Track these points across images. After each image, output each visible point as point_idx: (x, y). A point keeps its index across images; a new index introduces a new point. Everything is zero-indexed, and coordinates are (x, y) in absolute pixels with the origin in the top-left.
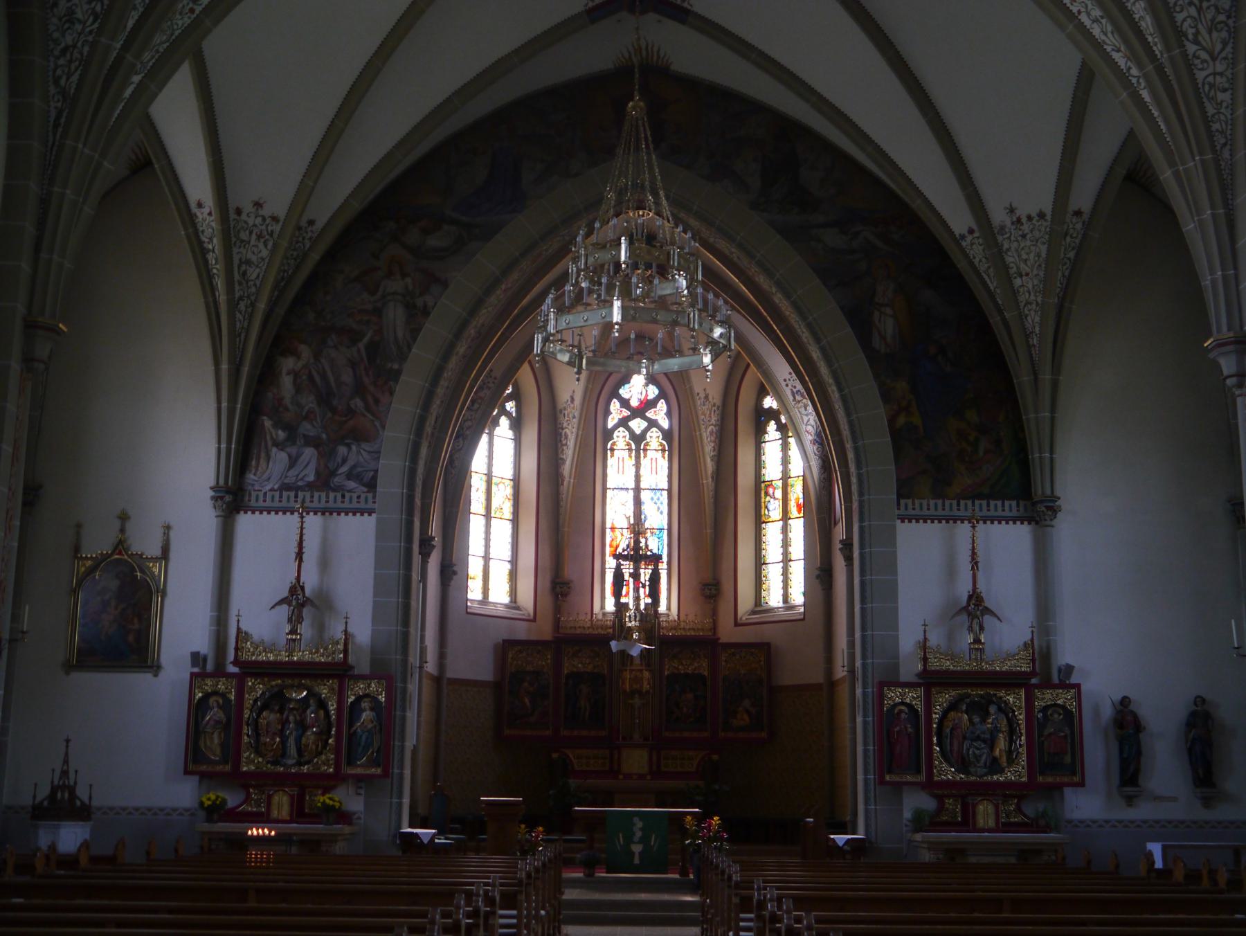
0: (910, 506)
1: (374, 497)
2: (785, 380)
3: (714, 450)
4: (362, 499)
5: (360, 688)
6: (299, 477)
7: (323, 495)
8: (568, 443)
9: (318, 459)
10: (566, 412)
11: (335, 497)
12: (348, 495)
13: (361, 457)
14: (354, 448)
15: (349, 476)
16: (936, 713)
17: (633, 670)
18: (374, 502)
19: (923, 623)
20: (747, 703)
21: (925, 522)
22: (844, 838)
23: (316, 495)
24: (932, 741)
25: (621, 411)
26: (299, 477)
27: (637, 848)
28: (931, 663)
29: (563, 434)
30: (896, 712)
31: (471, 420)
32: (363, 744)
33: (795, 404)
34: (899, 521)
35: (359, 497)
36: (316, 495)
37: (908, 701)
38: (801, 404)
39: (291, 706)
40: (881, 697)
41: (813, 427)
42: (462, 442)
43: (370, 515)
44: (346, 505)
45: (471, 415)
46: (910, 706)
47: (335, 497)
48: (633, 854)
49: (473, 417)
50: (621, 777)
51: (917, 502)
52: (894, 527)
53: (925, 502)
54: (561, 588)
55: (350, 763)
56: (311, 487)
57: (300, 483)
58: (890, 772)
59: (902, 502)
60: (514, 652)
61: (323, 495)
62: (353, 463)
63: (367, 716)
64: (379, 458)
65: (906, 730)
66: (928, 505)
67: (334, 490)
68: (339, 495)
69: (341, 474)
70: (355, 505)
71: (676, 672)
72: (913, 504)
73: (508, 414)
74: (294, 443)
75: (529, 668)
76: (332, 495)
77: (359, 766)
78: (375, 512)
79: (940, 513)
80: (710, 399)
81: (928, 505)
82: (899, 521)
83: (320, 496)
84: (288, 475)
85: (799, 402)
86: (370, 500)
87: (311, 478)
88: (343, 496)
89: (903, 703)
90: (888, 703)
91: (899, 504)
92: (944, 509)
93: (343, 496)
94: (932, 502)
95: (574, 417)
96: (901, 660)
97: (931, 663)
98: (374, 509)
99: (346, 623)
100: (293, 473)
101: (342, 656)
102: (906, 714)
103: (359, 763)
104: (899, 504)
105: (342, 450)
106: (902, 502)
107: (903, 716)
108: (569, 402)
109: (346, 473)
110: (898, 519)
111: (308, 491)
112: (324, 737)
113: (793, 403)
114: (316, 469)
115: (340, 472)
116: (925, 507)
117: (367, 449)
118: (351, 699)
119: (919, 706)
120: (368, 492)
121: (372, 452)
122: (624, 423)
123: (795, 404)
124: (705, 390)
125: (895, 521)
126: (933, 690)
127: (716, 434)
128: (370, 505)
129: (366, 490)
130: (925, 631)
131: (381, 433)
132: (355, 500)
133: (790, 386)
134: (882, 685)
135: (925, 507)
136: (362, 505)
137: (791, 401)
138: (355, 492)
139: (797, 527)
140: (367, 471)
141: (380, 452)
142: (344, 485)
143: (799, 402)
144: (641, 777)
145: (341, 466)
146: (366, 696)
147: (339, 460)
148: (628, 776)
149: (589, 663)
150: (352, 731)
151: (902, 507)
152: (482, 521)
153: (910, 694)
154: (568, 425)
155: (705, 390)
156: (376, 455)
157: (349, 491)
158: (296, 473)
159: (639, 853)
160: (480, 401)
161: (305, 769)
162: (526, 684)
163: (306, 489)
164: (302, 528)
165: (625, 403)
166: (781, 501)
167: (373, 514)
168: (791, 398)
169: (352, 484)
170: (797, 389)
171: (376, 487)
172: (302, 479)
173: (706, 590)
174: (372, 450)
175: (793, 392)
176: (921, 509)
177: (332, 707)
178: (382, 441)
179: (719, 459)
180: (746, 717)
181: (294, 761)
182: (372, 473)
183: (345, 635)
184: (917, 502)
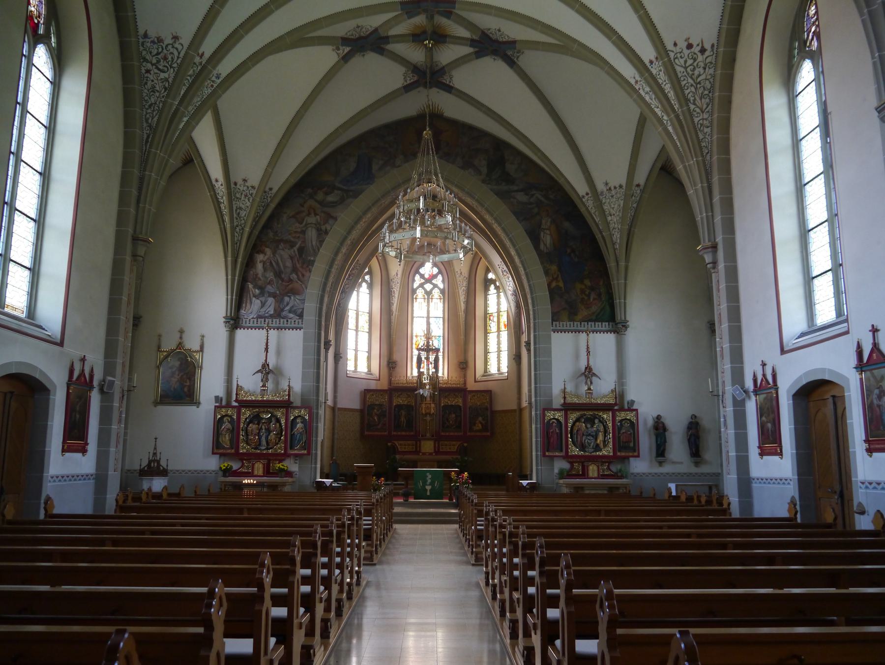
0: (558, 325)
1: (302, 322)
4: (296, 322)
5: (296, 412)
6: (266, 312)
7: (278, 320)
12: (289, 320)
14: (292, 298)
20: (480, 419)
23: (274, 320)
24: (568, 436)
27: (428, 488)
35: (295, 321)
36: (274, 320)
40: (544, 415)
44: (289, 325)
46: (557, 420)
47: (283, 322)
48: (427, 490)
51: (561, 323)
53: (565, 323)
56: (271, 316)
58: (548, 451)
59: (554, 323)
61: (278, 320)
66: (566, 325)
67: (283, 318)
68: (285, 320)
70: (293, 325)
72: (559, 324)
74: (263, 296)
75: (377, 403)
77: (296, 449)
80: (463, 274)
81: (566, 325)
85: (505, 275)
86: (300, 323)
87: (272, 312)
88: (287, 321)
89: (554, 419)
91: (552, 324)
93: (287, 321)
94: (568, 323)
96: (553, 398)
101: (287, 397)
104: (552, 324)
105: (286, 299)
106: (554, 323)
107: (554, 424)
112: (279, 436)
115: (285, 309)
119: (562, 419)
128: (300, 325)
129: (298, 318)
136: (296, 325)
139: (504, 335)
143: (505, 275)
144: (431, 454)
147: (285, 303)
148: (424, 454)
156: (303, 301)
157: (290, 319)
159: (430, 490)
161: (270, 451)
162: (375, 411)
165: (422, 276)
168: (502, 274)
169: (291, 315)
172: (267, 313)
174: (301, 299)
177: (283, 422)
180: (480, 425)
182: (301, 310)
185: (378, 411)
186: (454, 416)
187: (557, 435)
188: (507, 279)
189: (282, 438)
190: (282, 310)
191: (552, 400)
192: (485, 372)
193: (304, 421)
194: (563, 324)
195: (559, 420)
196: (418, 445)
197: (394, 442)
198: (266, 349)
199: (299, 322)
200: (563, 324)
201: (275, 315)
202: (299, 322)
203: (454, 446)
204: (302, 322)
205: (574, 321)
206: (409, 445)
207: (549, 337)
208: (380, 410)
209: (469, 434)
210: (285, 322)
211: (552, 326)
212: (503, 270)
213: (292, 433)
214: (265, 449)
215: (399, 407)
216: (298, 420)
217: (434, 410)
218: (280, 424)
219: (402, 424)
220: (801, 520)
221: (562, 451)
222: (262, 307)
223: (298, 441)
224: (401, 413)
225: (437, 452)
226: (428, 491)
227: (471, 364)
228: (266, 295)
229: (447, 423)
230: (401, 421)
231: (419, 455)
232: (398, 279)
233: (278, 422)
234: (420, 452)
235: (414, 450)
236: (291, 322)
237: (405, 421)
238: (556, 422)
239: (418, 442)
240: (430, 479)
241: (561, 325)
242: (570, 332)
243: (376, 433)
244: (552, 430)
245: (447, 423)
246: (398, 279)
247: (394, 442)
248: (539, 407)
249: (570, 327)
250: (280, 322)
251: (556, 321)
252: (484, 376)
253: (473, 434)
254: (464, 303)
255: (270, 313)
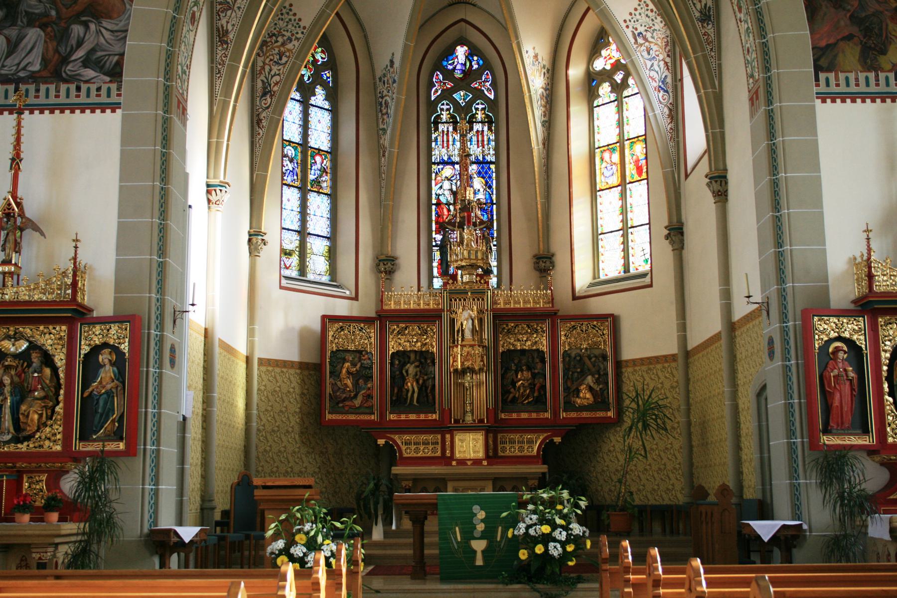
0: (833, 82)
1: (119, 89)
2: (625, 21)
3: (545, 116)
4: (104, 92)
5: (95, 335)
6: (22, 65)
7: (52, 87)
8: (389, 111)
9: (45, 42)
10: (386, 79)
11: (68, 90)
12: (84, 87)
13: (101, 38)
14: (93, 27)
15: (86, 63)
16: (886, 351)
17: (465, 346)
18: (119, 95)
19: (865, 228)
20: (589, 379)
21: (854, 101)
22: (776, 525)
23: (43, 87)
24: (883, 388)
25: (445, 84)
26: (22, 65)
27: (479, 545)
28: (879, 282)
29: (383, 103)
30: (830, 350)
31: (279, 75)
32: (100, 410)
33: (637, 47)
34: (820, 100)
35: (99, 89)
36: (43, 87)
37: (847, 335)
38: (643, 48)
39: (6, 363)
40: (807, 331)
41: (657, 73)
42: (269, 100)
43: (113, 111)
44: (83, 99)
45: (279, 70)
46: (849, 342)
47: (68, 90)
48: (475, 552)
49: (281, 72)
50: (454, 463)
51: (842, 76)
52: (814, 106)
53: (852, 76)
54: (384, 264)
55: (84, 437)
56: (34, 78)
57: (22, 74)
58: (826, 431)
59: (822, 76)
60: (335, 329)
61: (52, 87)
62: (92, 46)
63: (107, 373)
64: (126, 37)
65: (847, 376)
66: (857, 79)
67: (66, 81)
68: (73, 87)
69: (76, 60)
70: (93, 99)
71: (512, 348)
72: (837, 79)
73: (325, 85)
74: (14, 24)
75: (352, 347)
76: (63, 87)
77: (95, 440)
78: (120, 108)
79: (873, 88)
80: (540, 60)
81: (857, 79)
82: (820, 100)
83: (48, 90)
84: (5, 64)
85: (641, 45)
86: (114, 92)
87: (36, 67)
88: (78, 89)
89: (839, 339)
90: (819, 339)
91: (817, 79)
92: (877, 85)
93: (78, 89)
94: (862, 76)
95: (394, 82)
96: (830, 283)
97: (879, 282)
98: (120, 104)
99: (76, 247)
100: (11, 61)
101: (69, 291)
102: (845, 352)
103: (94, 437)
104: (817, 79)
105: (77, 30)
106: (822, 76)
107: (841, 355)
108: (389, 68)
109: (81, 60)
110: (817, 98)
111: (32, 83)
112: (51, 404)
113: (635, 46)
114: (43, 55)
115: (73, 58)
116: (852, 82)
117: (109, 27)
118: (85, 349)
119: (860, 340)
120: (111, 82)
121: (117, 31)
122: (447, 95)
123: (637, 47)
124: (534, 48)
125: (814, 102)
126: (880, 320)
127: (546, 98)
128: (114, 99)
129: (108, 79)
130: (868, 239)
131: (128, 6)
132: (94, 92)
133: (631, 27)
134: (807, 316)
135: (852, 82)
136: (104, 99)
137: (633, 43)
138: (94, 83)
139: (639, 193)
140: (110, 55)
141: (127, 31)
142: (79, 75)
143: (641, 45)
144: (477, 462)
145: (76, 50)
146: (105, 345)
147: (73, 42)
148: (462, 462)
149: (417, 342)
150: (86, 394)
151: (822, 81)
152: (312, 228)
153: (849, 326)
154: (388, 92)
155: (534, 48)
156: (122, 35)
157: (87, 82)
158: (16, 61)
159: (483, 552)
160: (288, 54)
161: (23, 447)
162: (347, 365)
163: (30, 81)
164: (18, 132)
165: (449, 75)
166: (619, 166)
167: (118, 110)
168: (633, 41)
169: (90, 73)
170: (638, 31)
171: (122, 76)
172: (24, 69)
173: (541, 262)
174: (116, 28)
175: (634, 34)
176: (848, 85)
177: (60, 360)
178: (130, 16)
179: (549, 124)
180: (588, 395)
181: (10, 436)
182: (116, 58)
183: (75, 263)
184: (842, 76)
185: (354, 365)
186: (527, 374)
187: (851, 384)
188: (645, 54)
189: (57, 409)
190: (65, 60)
191: (827, 287)
192: (594, 278)
193: (119, 361)
194: (847, 79)
195: (854, 342)
196: (448, 443)
197: (392, 436)
198: (13, 160)
199: (109, 90)
200: (847, 79)
201: (45, 74)
202: (109, 90)
203: (534, 444)
204: (119, 89)
205: (876, 68)
206: (426, 443)
207: (812, 112)
208: (359, 365)
209: (563, 415)
210: (73, 92)
211: (818, 85)
212: (636, 32)
213: (86, 394)
214: (8, 442)
215: (402, 357)
216: (104, 357)
217: (482, 361)
218: (55, 370)
219: (409, 395)
220: (410, 538)
221: (866, 431)
222: (10, 53)
223: (102, 415)
224: (407, 371)
225: (492, 455)
226: (479, 556)
227: (561, 260)
228: (22, 20)
229: (512, 390)
230: (408, 391)
231: (451, 465)
232: (393, 72)
233: (47, 366)
234: (452, 457)
235: (439, 454)
236: (89, 90)
237: (416, 389)
238: (845, 348)
239: (448, 436)
240: (482, 521)
241: (842, 82)
242: (868, 101)
243: (352, 417)
244: (836, 372)
245: (512, 390)
246: (393, 72)
247: (392, 436)
248: (790, 307)
249: (868, 85)
250: (58, 91)
251: (829, 70)
252: (592, 285)
253: (573, 415)
254: (543, 126)
255: (31, 68)
